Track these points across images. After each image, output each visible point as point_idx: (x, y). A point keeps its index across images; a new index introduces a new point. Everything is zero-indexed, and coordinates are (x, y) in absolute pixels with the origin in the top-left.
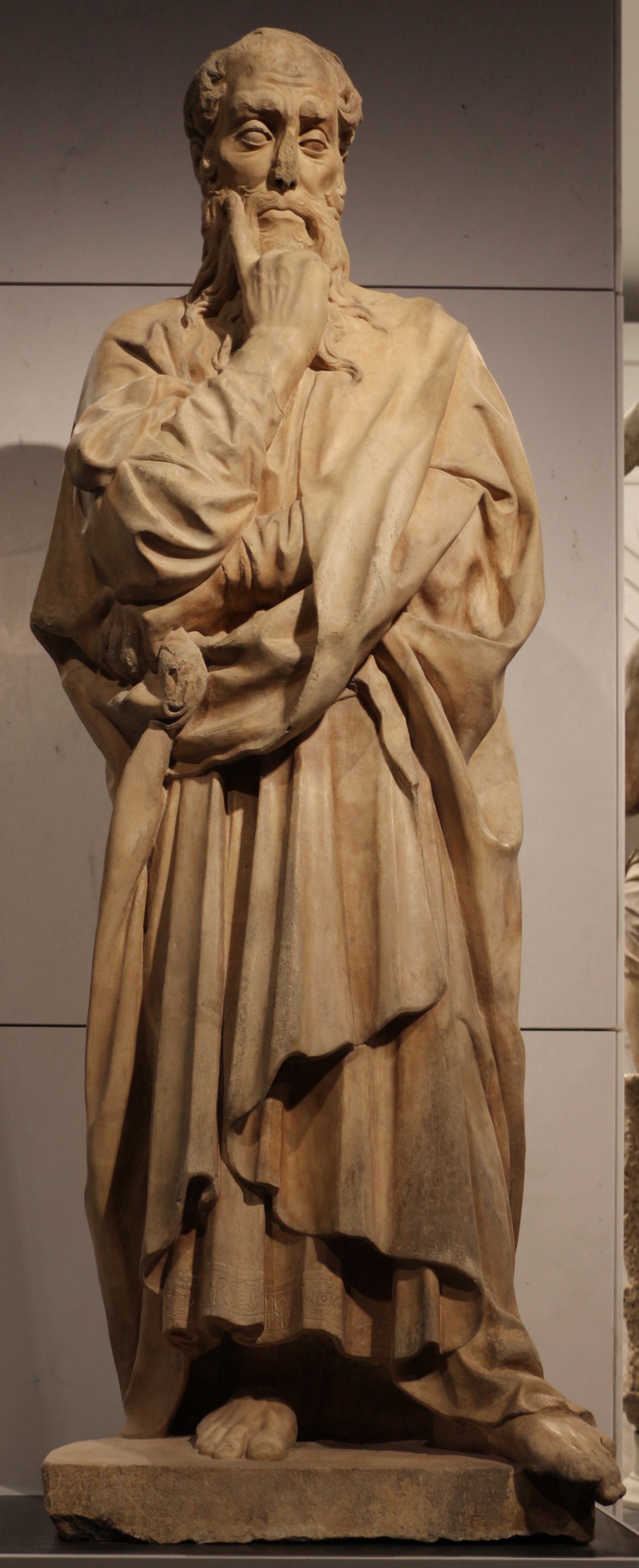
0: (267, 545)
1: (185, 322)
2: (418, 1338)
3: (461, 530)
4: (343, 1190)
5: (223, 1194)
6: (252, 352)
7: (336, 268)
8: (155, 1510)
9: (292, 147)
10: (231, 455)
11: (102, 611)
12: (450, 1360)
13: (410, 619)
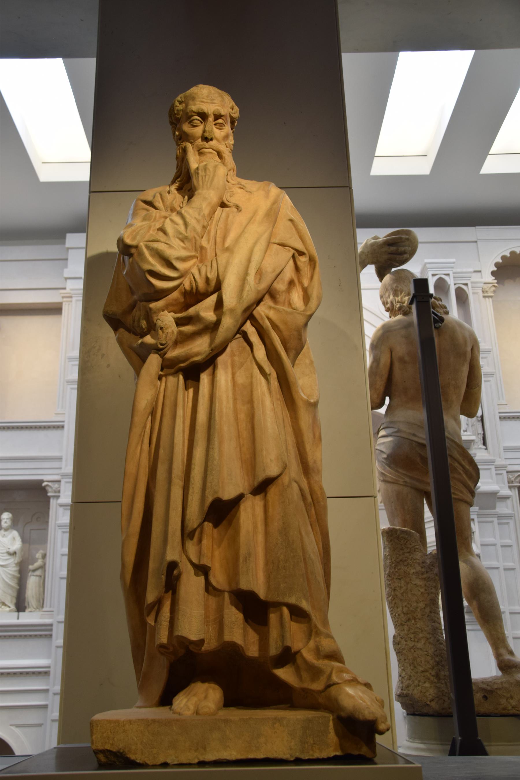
2: (281, 644)
3: (285, 267)
6: (195, 200)
7: (230, 170)
8: (148, 745)
9: (211, 125)
10: (186, 239)
11: (133, 306)
13: (264, 304)
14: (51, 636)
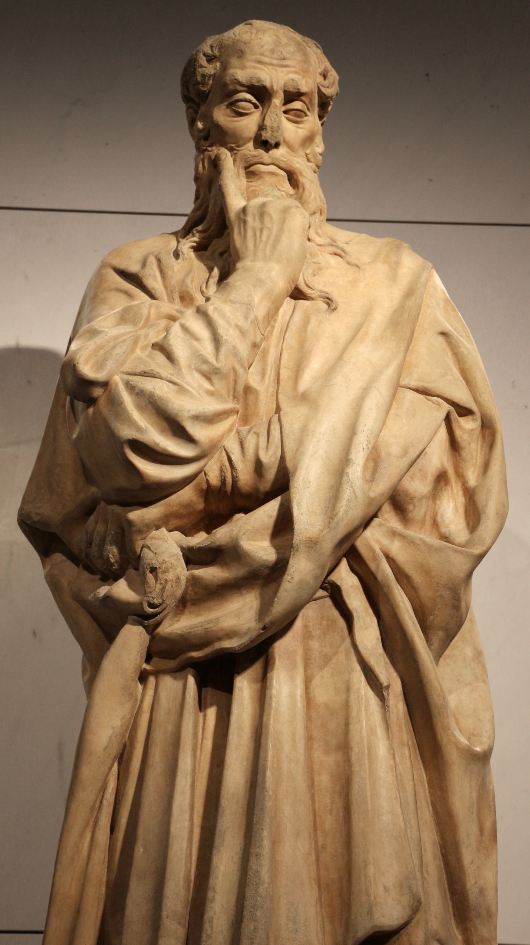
0: (247, 454)
6: (237, 284)
7: (314, 213)
9: (277, 115)
10: (216, 373)
13: (381, 525)
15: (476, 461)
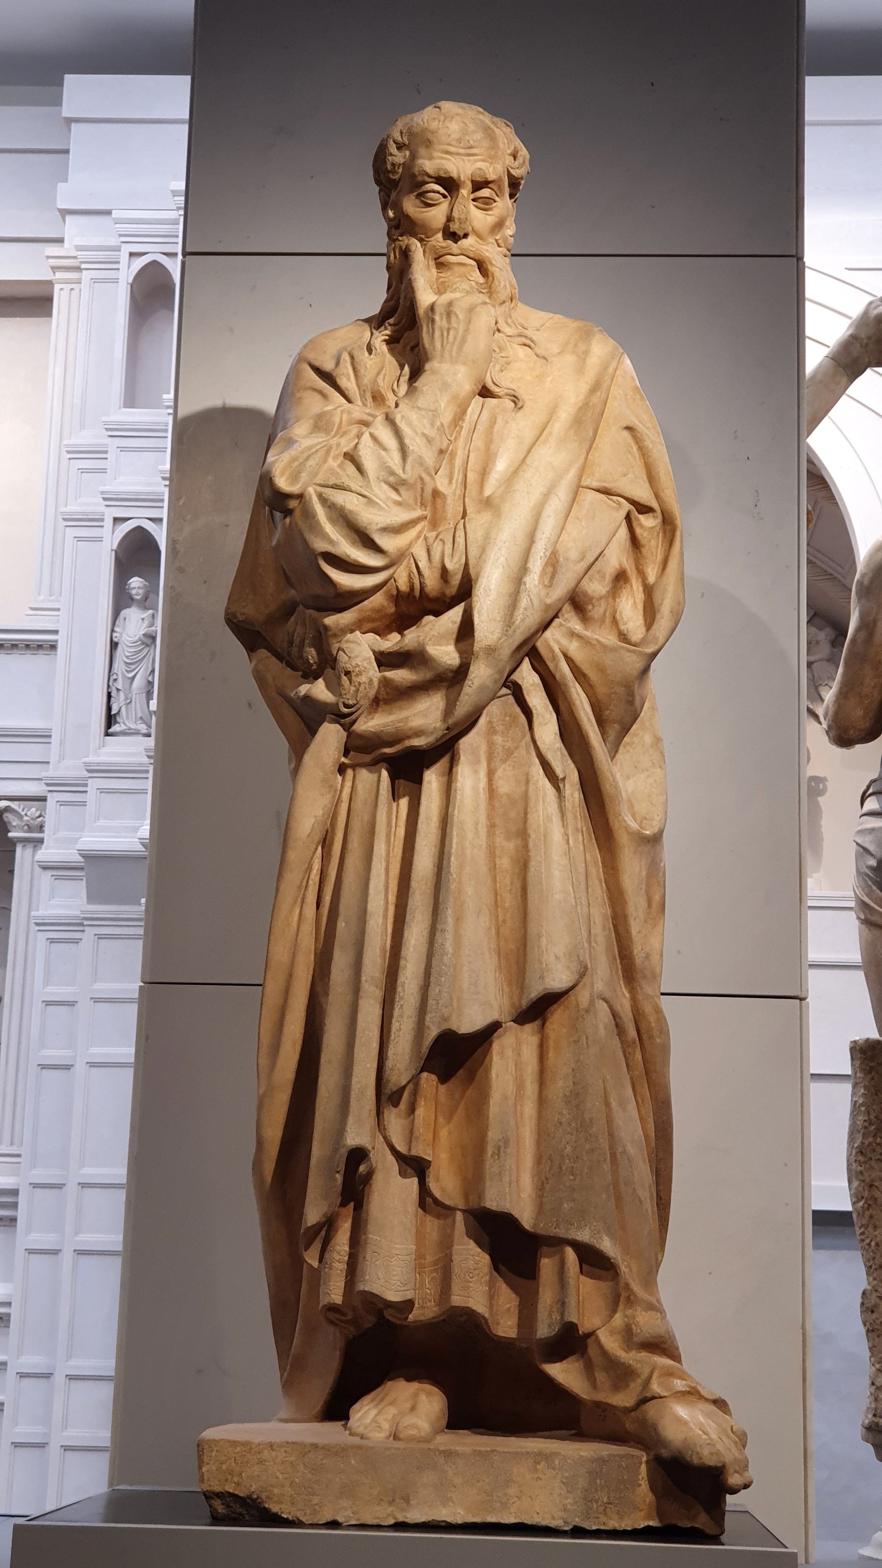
0: (433, 561)
1: (370, 350)
2: (559, 1318)
4: (490, 1166)
5: (380, 1167)
10: (403, 484)
12: (590, 1341)
13: (561, 625)
14: (13, 1220)
15: (656, 557)
